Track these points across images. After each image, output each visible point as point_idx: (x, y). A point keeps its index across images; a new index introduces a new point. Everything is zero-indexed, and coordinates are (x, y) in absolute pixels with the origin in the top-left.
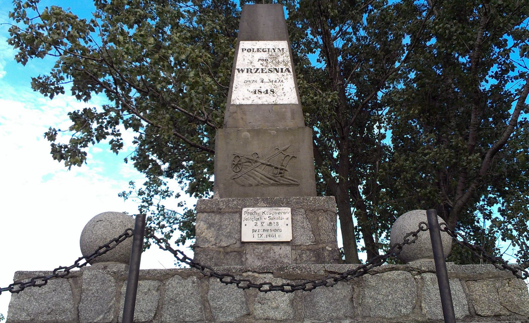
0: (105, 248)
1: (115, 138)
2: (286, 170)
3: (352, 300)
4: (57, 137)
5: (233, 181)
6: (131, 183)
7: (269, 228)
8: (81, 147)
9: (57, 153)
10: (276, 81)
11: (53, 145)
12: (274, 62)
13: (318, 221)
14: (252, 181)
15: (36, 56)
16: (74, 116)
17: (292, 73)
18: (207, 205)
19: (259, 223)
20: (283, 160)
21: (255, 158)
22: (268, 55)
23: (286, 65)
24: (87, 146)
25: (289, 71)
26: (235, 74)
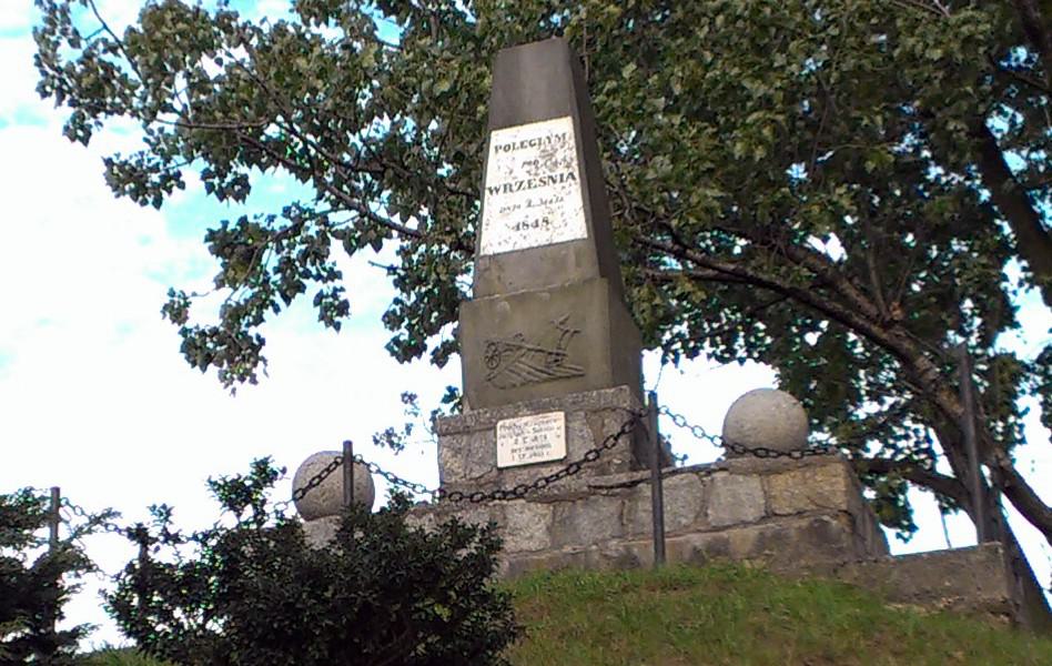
0: (317, 480)
1: (328, 288)
2: (564, 355)
3: (621, 516)
4: (191, 311)
5: (489, 383)
6: (409, 398)
7: (534, 444)
8: (248, 325)
9: (197, 350)
10: (551, 202)
11: (184, 332)
12: (549, 163)
13: (603, 425)
14: (517, 380)
15: (108, 113)
16: (221, 242)
17: (578, 180)
18: (450, 425)
19: (520, 439)
20: (561, 340)
21: (517, 342)
22: (538, 152)
23: (568, 166)
24: (262, 320)
25: (574, 178)
26: (486, 197)
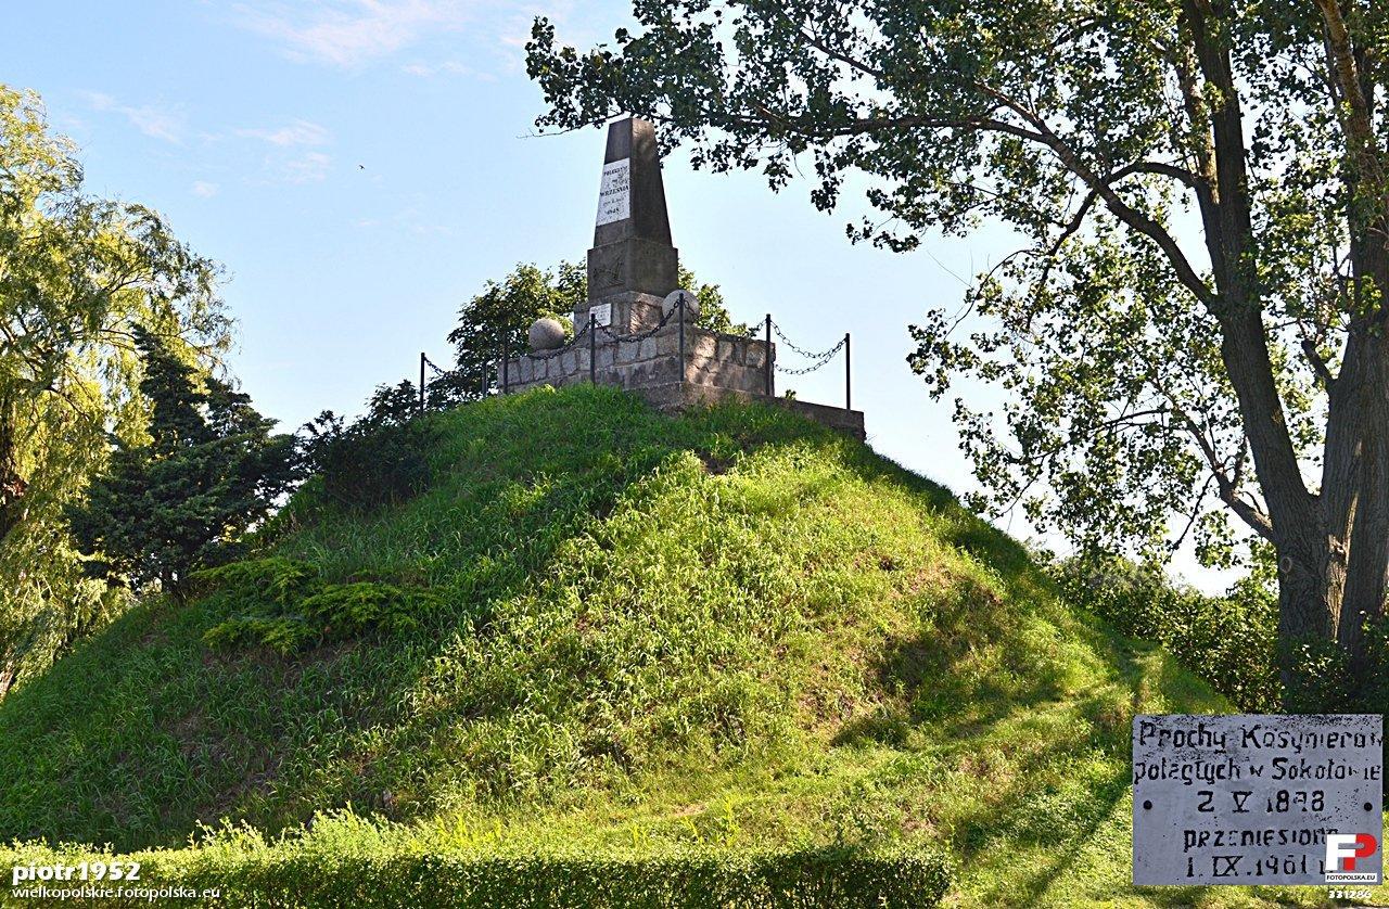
7: (1274, 822)
16: (800, 96)
19: (1222, 793)
